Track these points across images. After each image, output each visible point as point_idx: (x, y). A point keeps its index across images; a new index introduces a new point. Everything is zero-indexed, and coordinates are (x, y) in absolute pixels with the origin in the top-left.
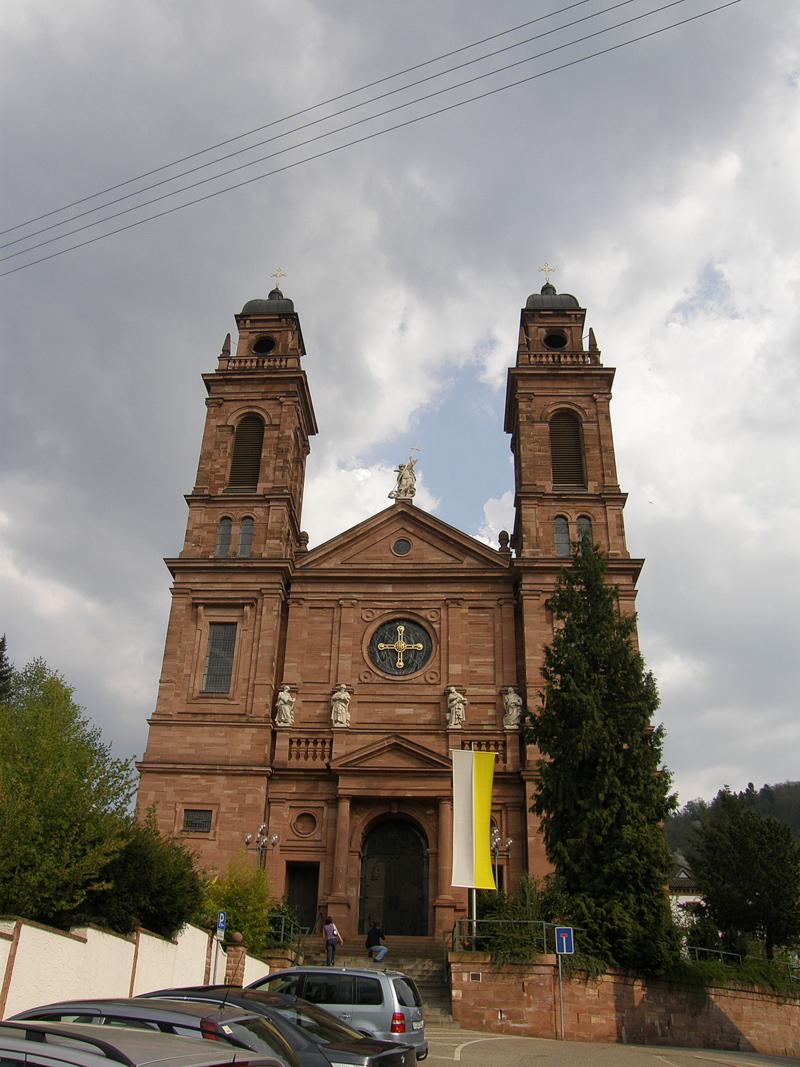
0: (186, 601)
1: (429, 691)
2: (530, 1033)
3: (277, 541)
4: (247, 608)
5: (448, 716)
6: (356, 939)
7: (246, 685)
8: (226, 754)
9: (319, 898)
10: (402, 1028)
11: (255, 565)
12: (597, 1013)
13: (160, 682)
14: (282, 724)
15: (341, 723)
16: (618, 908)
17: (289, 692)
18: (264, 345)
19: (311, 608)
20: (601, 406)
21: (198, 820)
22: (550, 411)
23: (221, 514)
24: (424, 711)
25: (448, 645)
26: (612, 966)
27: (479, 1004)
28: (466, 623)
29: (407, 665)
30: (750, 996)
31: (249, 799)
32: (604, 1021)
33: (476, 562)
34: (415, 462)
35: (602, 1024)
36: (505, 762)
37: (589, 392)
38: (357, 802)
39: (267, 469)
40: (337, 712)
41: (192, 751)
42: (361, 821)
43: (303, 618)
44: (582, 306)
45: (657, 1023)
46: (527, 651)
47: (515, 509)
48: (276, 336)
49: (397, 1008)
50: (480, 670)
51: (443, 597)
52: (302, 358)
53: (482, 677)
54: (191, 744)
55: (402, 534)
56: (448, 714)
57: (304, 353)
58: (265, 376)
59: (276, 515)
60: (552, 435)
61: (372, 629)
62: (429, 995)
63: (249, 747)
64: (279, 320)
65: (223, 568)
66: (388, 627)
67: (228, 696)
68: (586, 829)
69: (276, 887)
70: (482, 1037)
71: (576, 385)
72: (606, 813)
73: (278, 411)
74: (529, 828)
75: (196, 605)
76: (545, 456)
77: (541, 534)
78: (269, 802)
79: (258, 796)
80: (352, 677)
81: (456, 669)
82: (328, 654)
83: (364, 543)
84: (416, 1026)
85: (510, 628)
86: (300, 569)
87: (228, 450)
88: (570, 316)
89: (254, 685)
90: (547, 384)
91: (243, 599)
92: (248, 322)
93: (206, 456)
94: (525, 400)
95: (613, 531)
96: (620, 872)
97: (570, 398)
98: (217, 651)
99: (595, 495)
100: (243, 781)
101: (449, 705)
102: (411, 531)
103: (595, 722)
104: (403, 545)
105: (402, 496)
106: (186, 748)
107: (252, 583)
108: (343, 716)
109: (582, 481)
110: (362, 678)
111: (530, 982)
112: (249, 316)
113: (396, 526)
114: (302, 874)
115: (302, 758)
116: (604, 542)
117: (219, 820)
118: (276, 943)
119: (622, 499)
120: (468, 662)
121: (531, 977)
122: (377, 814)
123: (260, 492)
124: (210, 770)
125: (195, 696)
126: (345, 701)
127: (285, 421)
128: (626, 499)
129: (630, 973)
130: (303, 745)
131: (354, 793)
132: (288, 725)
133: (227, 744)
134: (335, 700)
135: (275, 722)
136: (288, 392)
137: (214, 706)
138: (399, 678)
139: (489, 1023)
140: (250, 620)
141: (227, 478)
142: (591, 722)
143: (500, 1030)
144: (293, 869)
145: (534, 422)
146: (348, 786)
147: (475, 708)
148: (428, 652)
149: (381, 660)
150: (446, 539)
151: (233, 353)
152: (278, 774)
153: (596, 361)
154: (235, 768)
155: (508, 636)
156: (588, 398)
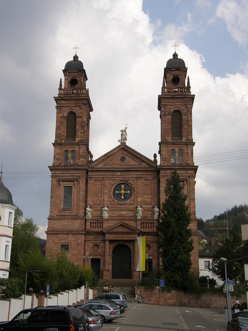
0: (55, 180)
1: (131, 206)
2: (153, 304)
3: (84, 159)
4: (75, 182)
6: (111, 280)
7: (76, 206)
10: (123, 303)
13: (50, 206)
18: (73, 82)
21: (66, 247)
22: (172, 111)
23: (64, 149)
24: (130, 212)
26: (175, 289)
28: (143, 184)
30: (215, 295)
34: (127, 128)
36: (154, 229)
37: (185, 103)
38: (111, 241)
39: (78, 133)
40: (104, 214)
41: (62, 227)
42: (113, 246)
44: (186, 67)
45: (186, 302)
46: (161, 195)
48: (78, 78)
49: (122, 300)
50: (147, 200)
51: (136, 176)
52: (91, 113)
53: (147, 202)
54: (61, 225)
56: (137, 214)
57: (87, 79)
58: (76, 98)
59: (82, 150)
60: (172, 119)
62: (130, 296)
63: (78, 226)
64: (79, 72)
65: (67, 169)
66: (119, 185)
68: (170, 255)
69: (88, 266)
71: (181, 101)
73: (81, 111)
75: (60, 181)
76: (169, 128)
77: (167, 156)
78: (85, 242)
79: (82, 240)
80: (108, 202)
81: (139, 199)
82: (101, 195)
83: (111, 158)
85: (156, 186)
86: (91, 168)
90: (171, 100)
92: (67, 72)
93: (58, 128)
94: (163, 107)
95: (190, 155)
97: (179, 106)
98: (66, 194)
99: (185, 143)
100: (77, 236)
101: (138, 211)
102: (126, 154)
104: (123, 159)
106: (60, 226)
107: (77, 174)
108: (106, 215)
109: (181, 136)
110: (111, 203)
112: (67, 70)
113: (121, 152)
114: (96, 262)
115: (94, 228)
116: (186, 159)
119: (193, 144)
120: (143, 197)
123: (77, 141)
124: (68, 233)
125: (61, 210)
126: (106, 211)
127: (83, 115)
128: (195, 144)
129: (180, 290)
130: (94, 224)
131: (110, 239)
132: (89, 218)
133: (72, 225)
134: (103, 210)
136: (84, 104)
137: (67, 213)
140: (76, 185)
141: (65, 136)
142: (172, 227)
143: (146, 303)
144: (93, 260)
145: (166, 115)
146: (108, 237)
148: (131, 193)
150: (137, 157)
151: (63, 88)
152: (87, 233)
153: (189, 92)
154: (75, 232)
156: (185, 106)
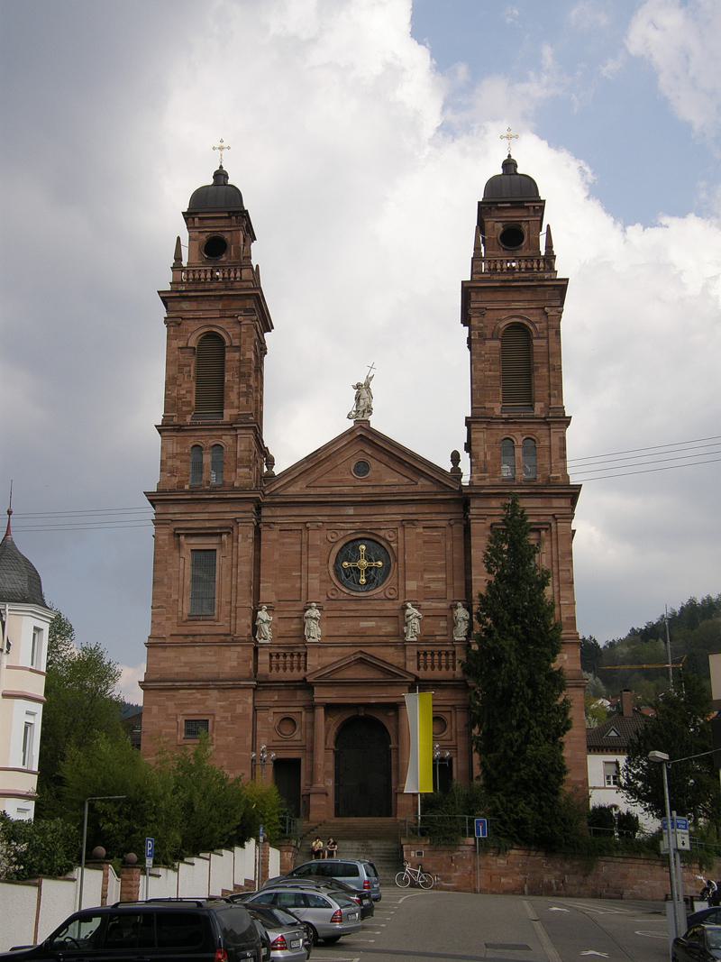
0: (166, 531)
1: (389, 605)
2: (456, 889)
3: (247, 470)
4: (224, 537)
6: (332, 821)
8: (217, 671)
9: (302, 788)
10: (368, 887)
11: (228, 496)
12: (505, 876)
14: (261, 641)
16: (522, 804)
17: (266, 610)
18: (213, 248)
19: (280, 530)
22: (501, 326)
23: (191, 442)
24: (385, 623)
25: (405, 563)
28: (420, 541)
29: (369, 581)
31: (239, 709)
32: (511, 881)
33: (429, 483)
35: (509, 883)
37: (541, 304)
38: (330, 708)
40: (309, 629)
41: (186, 669)
42: (336, 720)
45: (553, 881)
48: (227, 236)
49: (366, 878)
50: (433, 586)
53: (435, 592)
54: (185, 663)
55: (361, 457)
58: (222, 293)
59: (244, 444)
60: (503, 350)
63: (235, 664)
64: (229, 217)
66: (351, 545)
67: (214, 618)
68: (502, 745)
72: (517, 734)
75: (179, 535)
76: (495, 376)
77: (488, 458)
78: (255, 710)
80: (321, 594)
81: (412, 585)
83: (327, 466)
84: (375, 886)
86: (268, 494)
87: (192, 374)
88: (528, 207)
89: (236, 608)
90: (500, 296)
91: (221, 528)
92: (196, 220)
93: (171, 382)
95: (555, 455)
96: (523, 779)
100: (232, 694)
102: (369, 453)
103: (511, 664)
104: (362, 468)
107: (227, 513)
108: (315, 632)
111: (457, 857)
114: (287, 770)
116: (547, 466)
118: (283, 835)
119: (566, 421)
120: (422, 578)
121: (457, 854)
122: (346, 717)
123: (226, 419)
124: (205, 684)
125: (184, 619)
126: (316, 619)
127: (245, 341)
131: (329, 701)
134: (307, 618)
135: (256, 639)
136: (246, 310)
137: (201, 627)
138: (361, 594)
141: (194, 404)
143: (435, 888)
145: (485, 339)
146: (323, 695)
147: (428, 620)
148: (387, 568)
149: (347, 577)
150: (402, 462)
151: (184, 263)
152: (262, 685)
155: (459, 555)
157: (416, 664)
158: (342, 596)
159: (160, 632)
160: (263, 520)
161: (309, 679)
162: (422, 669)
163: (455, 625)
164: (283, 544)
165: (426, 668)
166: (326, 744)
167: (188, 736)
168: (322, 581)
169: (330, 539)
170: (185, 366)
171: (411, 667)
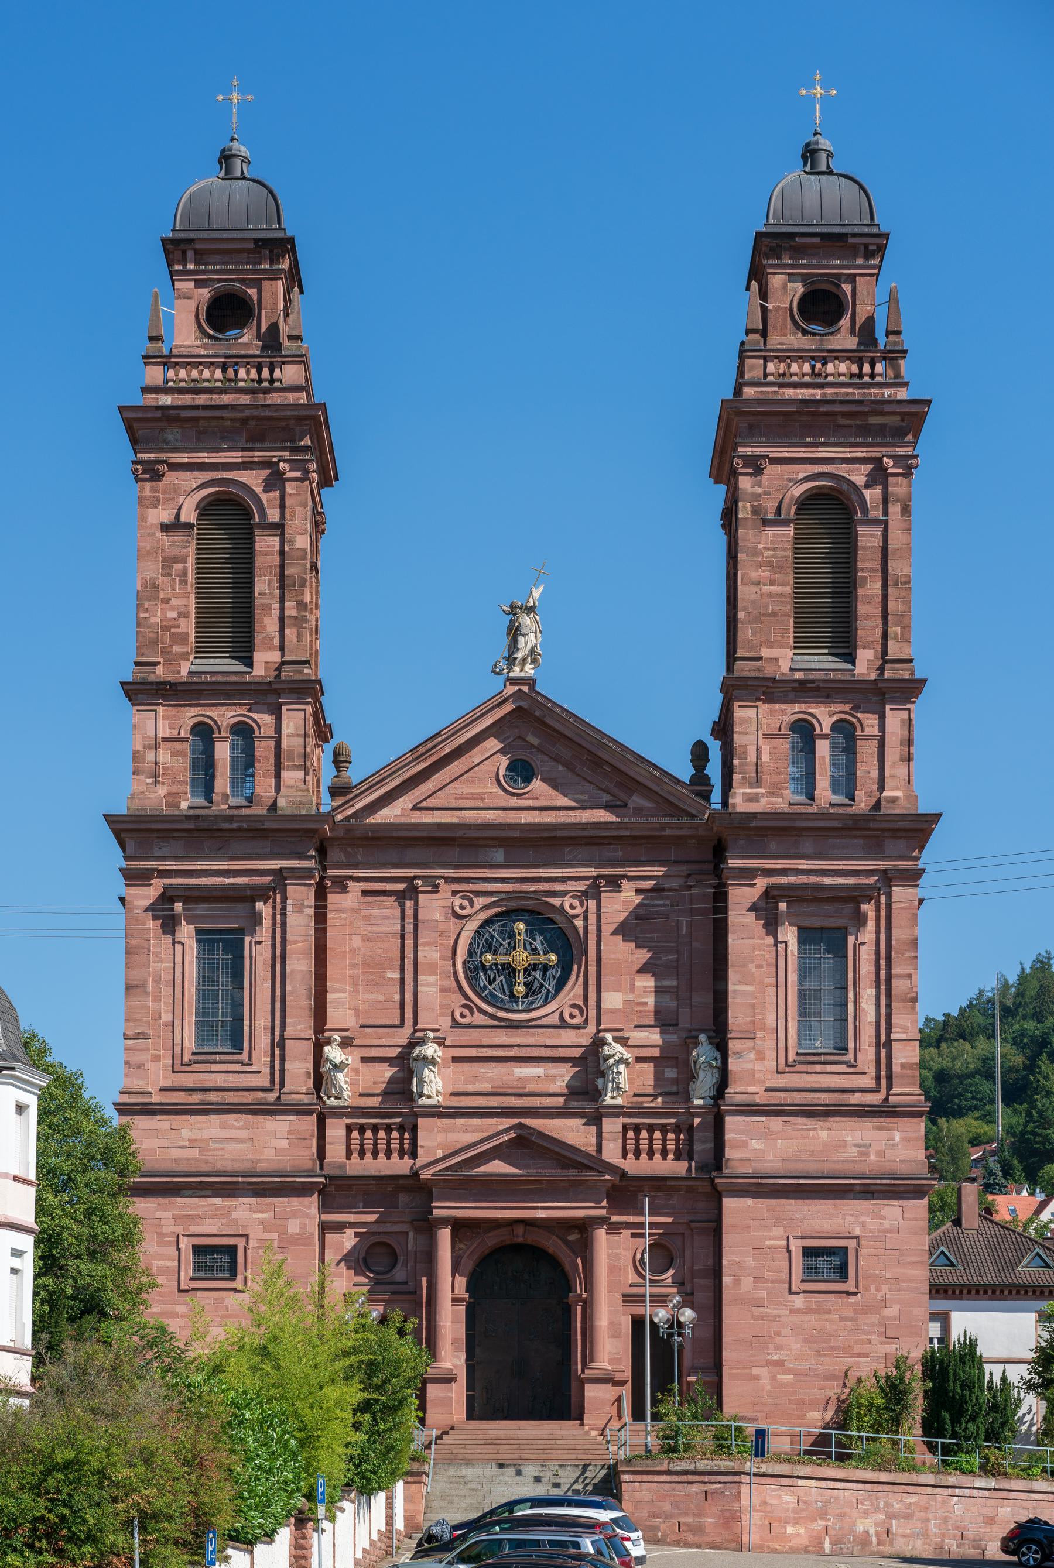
1: (568, 1037)
5: (600, 1082)
12: (796, 1522)
14: (332, 1102)
15: (429, 1097)
17: (339, 1045)
20: (897, 485)
27: (653, 1515)
31: (294, 1226)
32: (802, 1531)
35: (799, 1535)
37: (875, 452)
38: (460, 1227)
39: (267, 621)
41: (194, 1153)
43: (352, 910)
45: (872, 1531)
47: (721, 696)
54: (190, 1141)
60: (799, 543)
61: (472, 926)
70: (658, 1550)
74: (724, 1263)
76: (782, 594)
88: (854, 246)
105: (516, 672)
117: (249, 1260)
125: (186, 1059)
139: (664, 1536)
141: (192, 639)
150: (597, 762)
157: (620, 1145)
158: (479, 1019)
159: (140, 1082)
160: (331, 872)
161: (426, 1175)
162: (630, 1156)
163: (692, 1077)
164: (368, 918)
165: (637, 1156)
166: (453, 1291)
167: (201, 1275)
168: (443, 990)
169: (457, 909)
170: (176, 561)
171: (611, 1153)
